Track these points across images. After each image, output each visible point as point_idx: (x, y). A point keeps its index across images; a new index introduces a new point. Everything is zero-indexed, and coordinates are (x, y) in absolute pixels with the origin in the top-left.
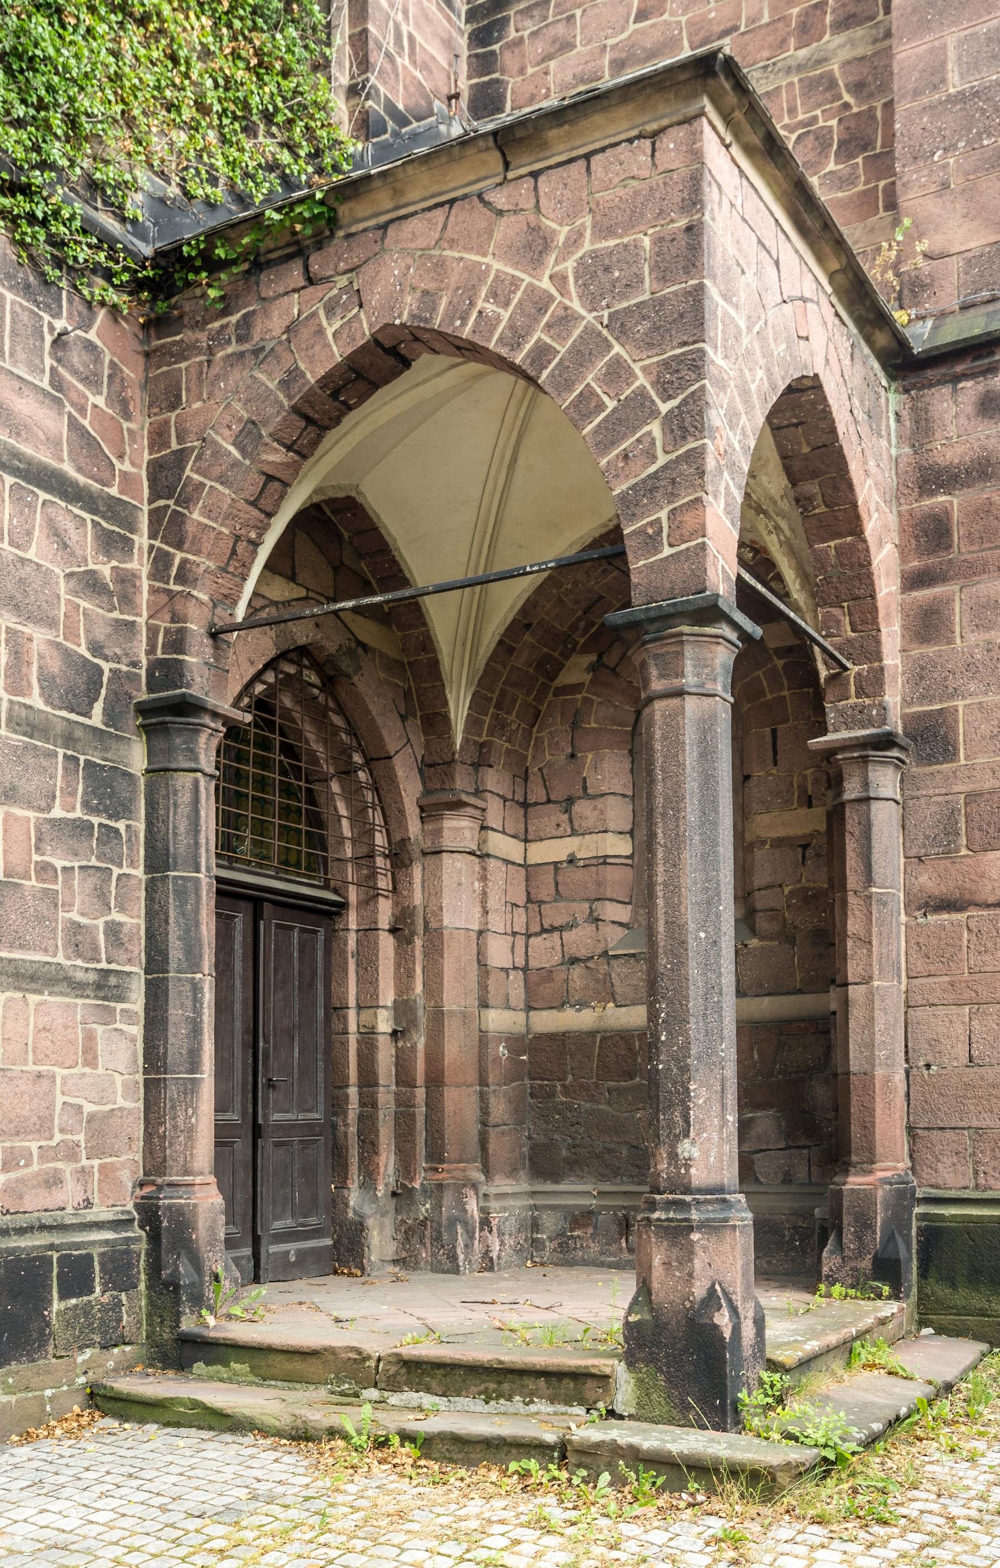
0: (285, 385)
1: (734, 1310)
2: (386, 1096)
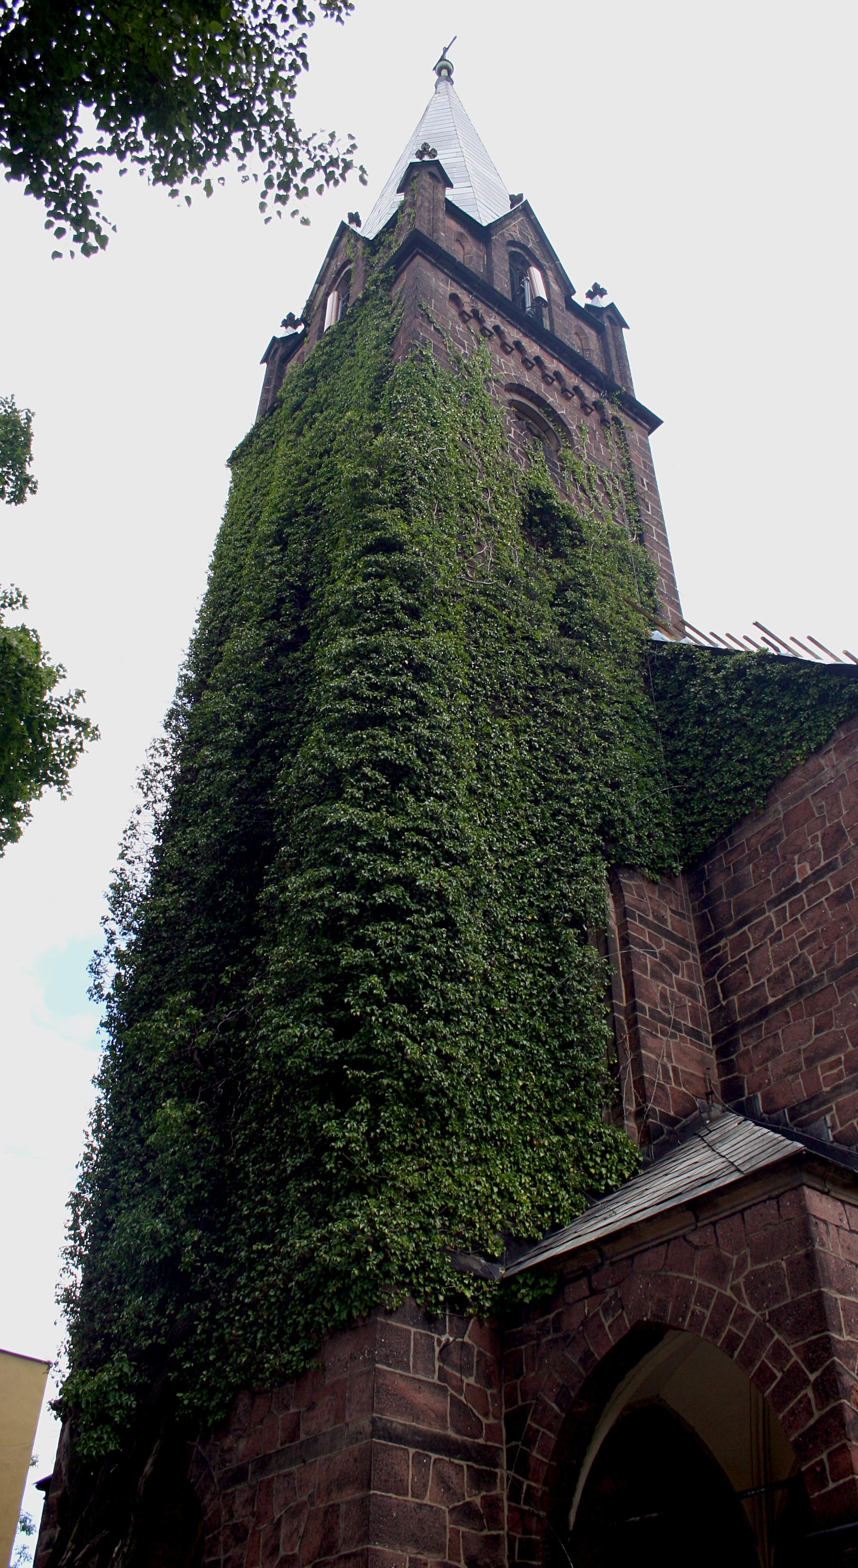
0: (582, 1361)
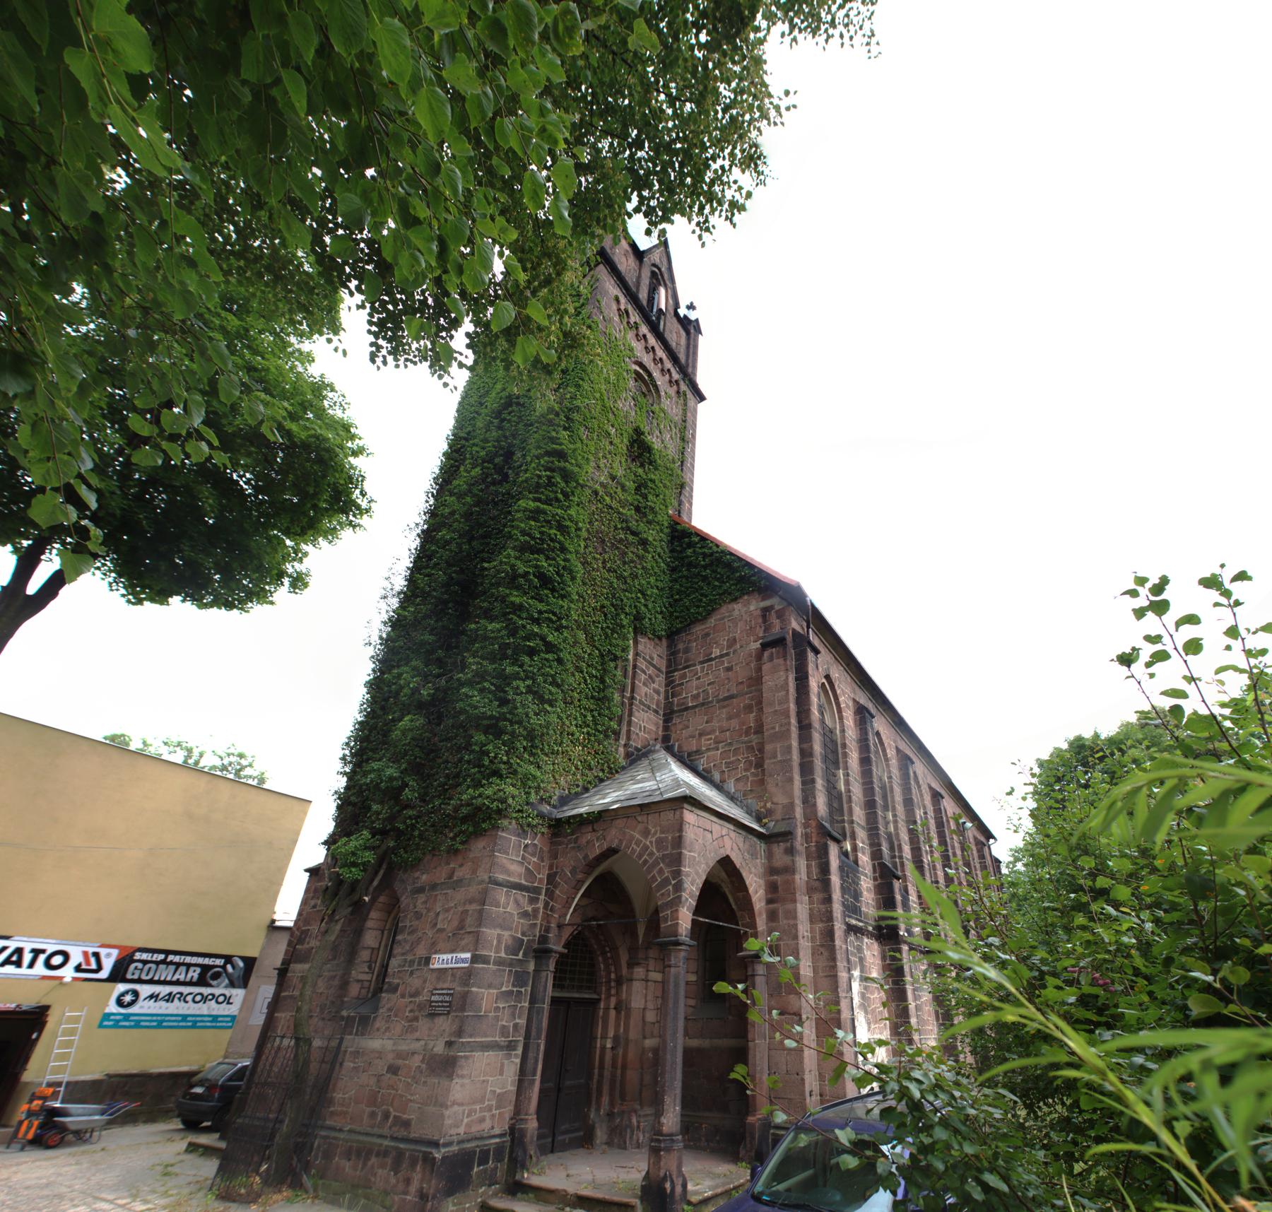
1: (672, 1182)
2: (607, 1074)
